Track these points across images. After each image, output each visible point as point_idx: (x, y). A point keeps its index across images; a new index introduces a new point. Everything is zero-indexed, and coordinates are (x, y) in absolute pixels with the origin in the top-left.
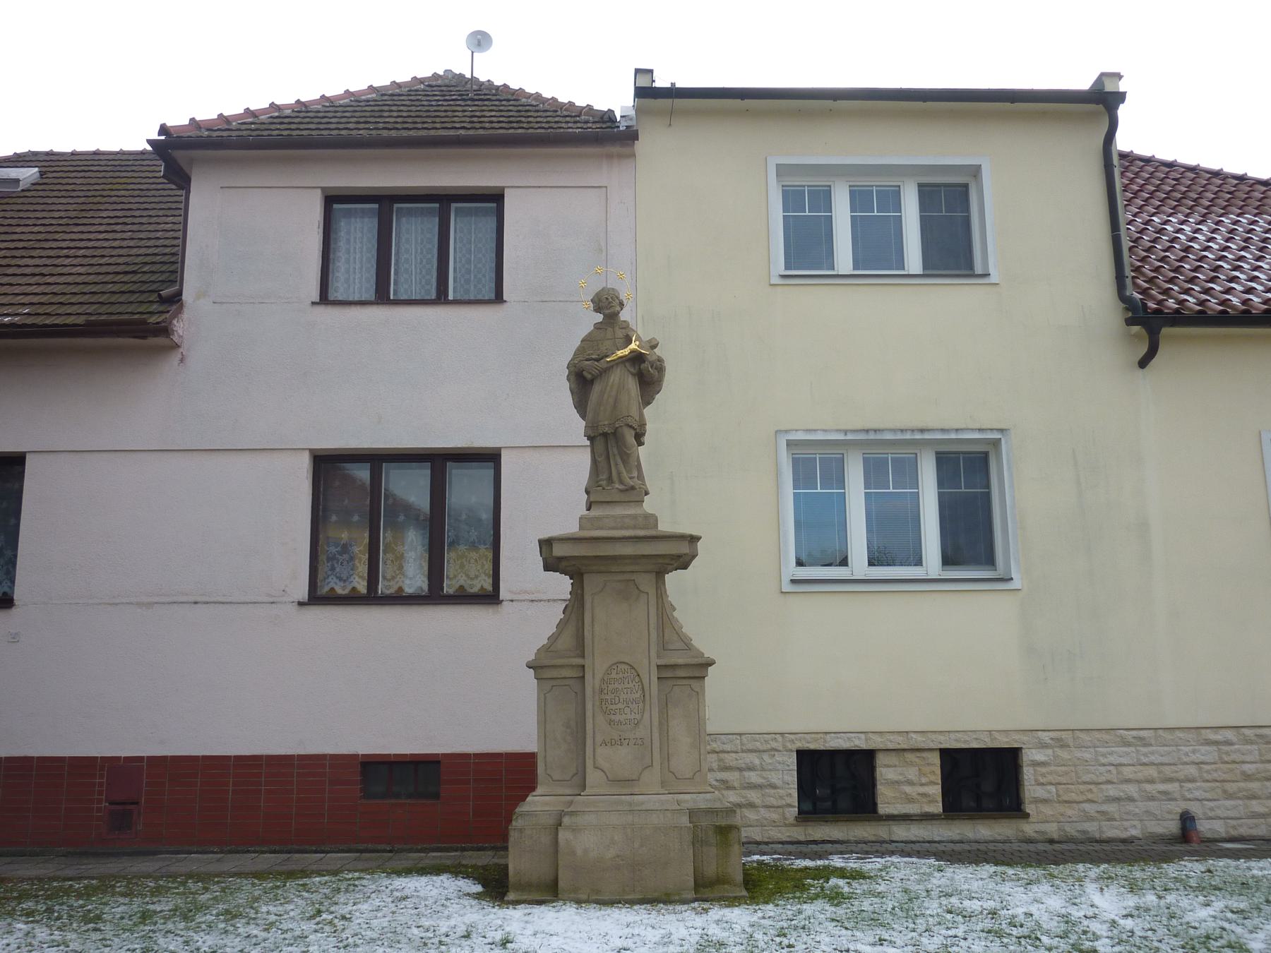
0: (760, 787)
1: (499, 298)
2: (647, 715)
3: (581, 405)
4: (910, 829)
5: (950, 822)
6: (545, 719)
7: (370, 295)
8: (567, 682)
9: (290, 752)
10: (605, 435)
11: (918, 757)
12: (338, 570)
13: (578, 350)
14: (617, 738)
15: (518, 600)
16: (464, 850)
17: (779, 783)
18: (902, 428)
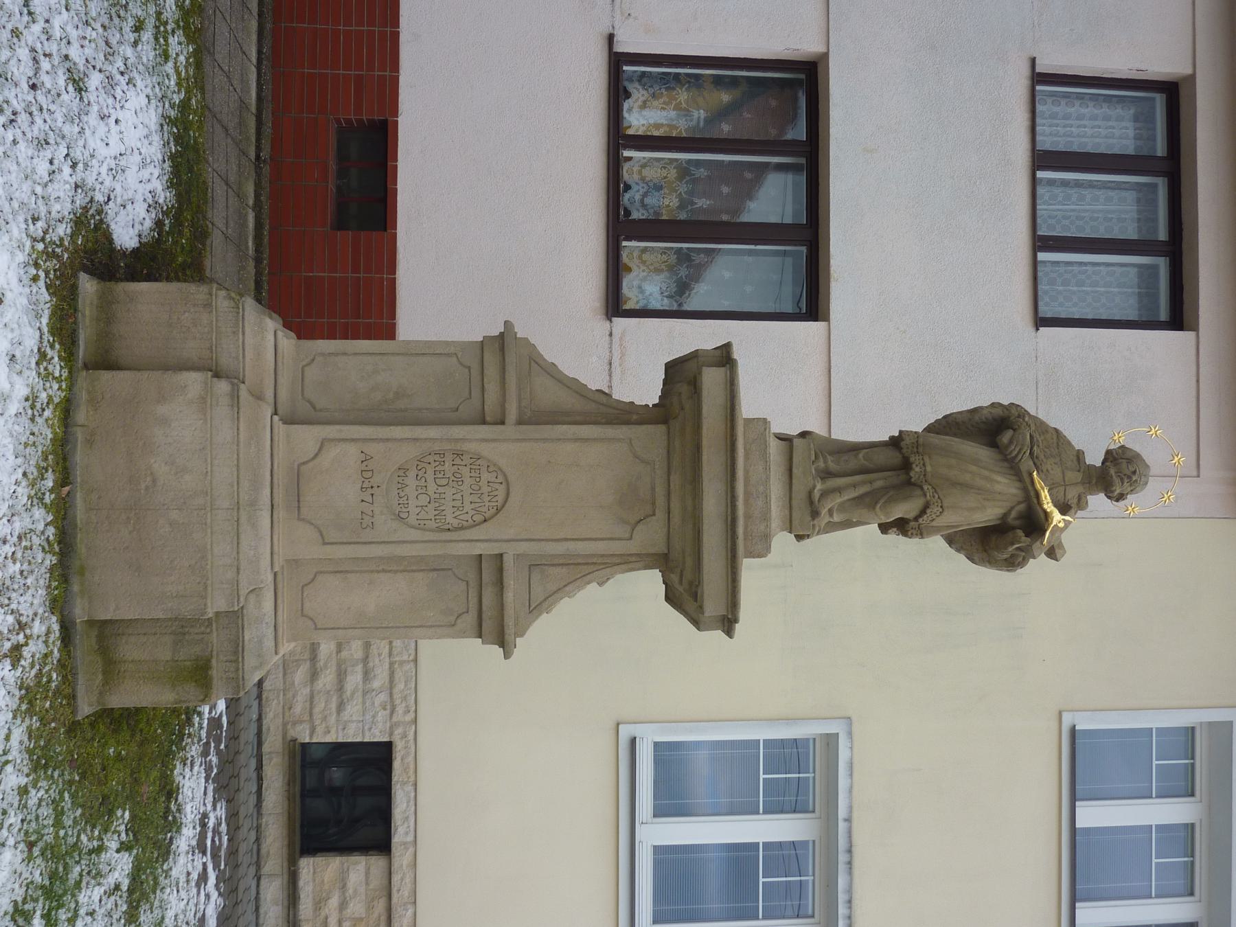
0: (340, 688)
1: (1041, 322)
2: (414, 534)
3: (949, 426)
7: (1045, 143)
8: (476, 393)
10: (906, 466)
11: (380, 917)
13: (1042, 423)
14: (375, 481)
15: (611, 343)
16: (258, 261)
17: (346, 715)
18: (853, 902)
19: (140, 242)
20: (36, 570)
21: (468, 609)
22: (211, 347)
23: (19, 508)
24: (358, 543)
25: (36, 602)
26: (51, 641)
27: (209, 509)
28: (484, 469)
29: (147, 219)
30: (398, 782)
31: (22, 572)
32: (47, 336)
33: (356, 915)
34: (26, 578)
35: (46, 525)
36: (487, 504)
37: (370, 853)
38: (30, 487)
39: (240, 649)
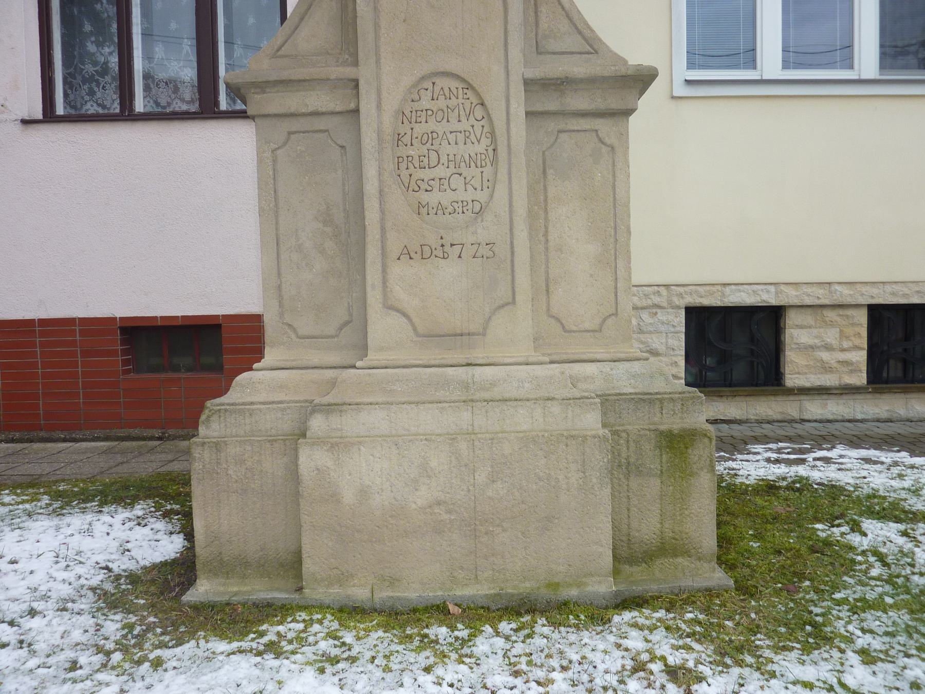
2: (501, 191)
4: (827, 404)
5: (878, 395)
6: (276, 205)
8: (320, 123)
9: (28, 316)
11: (840, 315)
12: (99, 95)
14: (433, 241)
17: (661, 348)
19: (179, 533)
20: (558, 646)
21: (593, 130)
22: (269, 441)
23: (474, 677)
24: (512, 261)
25: (601, 647)
26: (648, 622)
27: (473, 436)
28: (416, 106)
29: (153, 526)
30: (721, 301)
31: (564, 669)
32: (245, 645)
33: (837, 336)
34: (571, 662)
35: (498, 634)
36: (460, 101)
37: (782, 325)
38: (446, 660)
39: (646, 397)
